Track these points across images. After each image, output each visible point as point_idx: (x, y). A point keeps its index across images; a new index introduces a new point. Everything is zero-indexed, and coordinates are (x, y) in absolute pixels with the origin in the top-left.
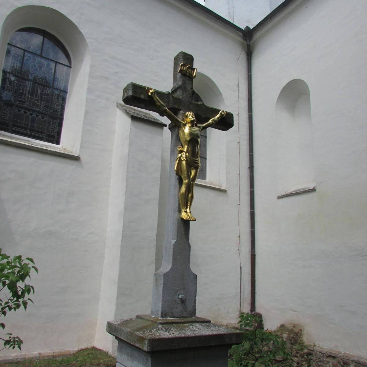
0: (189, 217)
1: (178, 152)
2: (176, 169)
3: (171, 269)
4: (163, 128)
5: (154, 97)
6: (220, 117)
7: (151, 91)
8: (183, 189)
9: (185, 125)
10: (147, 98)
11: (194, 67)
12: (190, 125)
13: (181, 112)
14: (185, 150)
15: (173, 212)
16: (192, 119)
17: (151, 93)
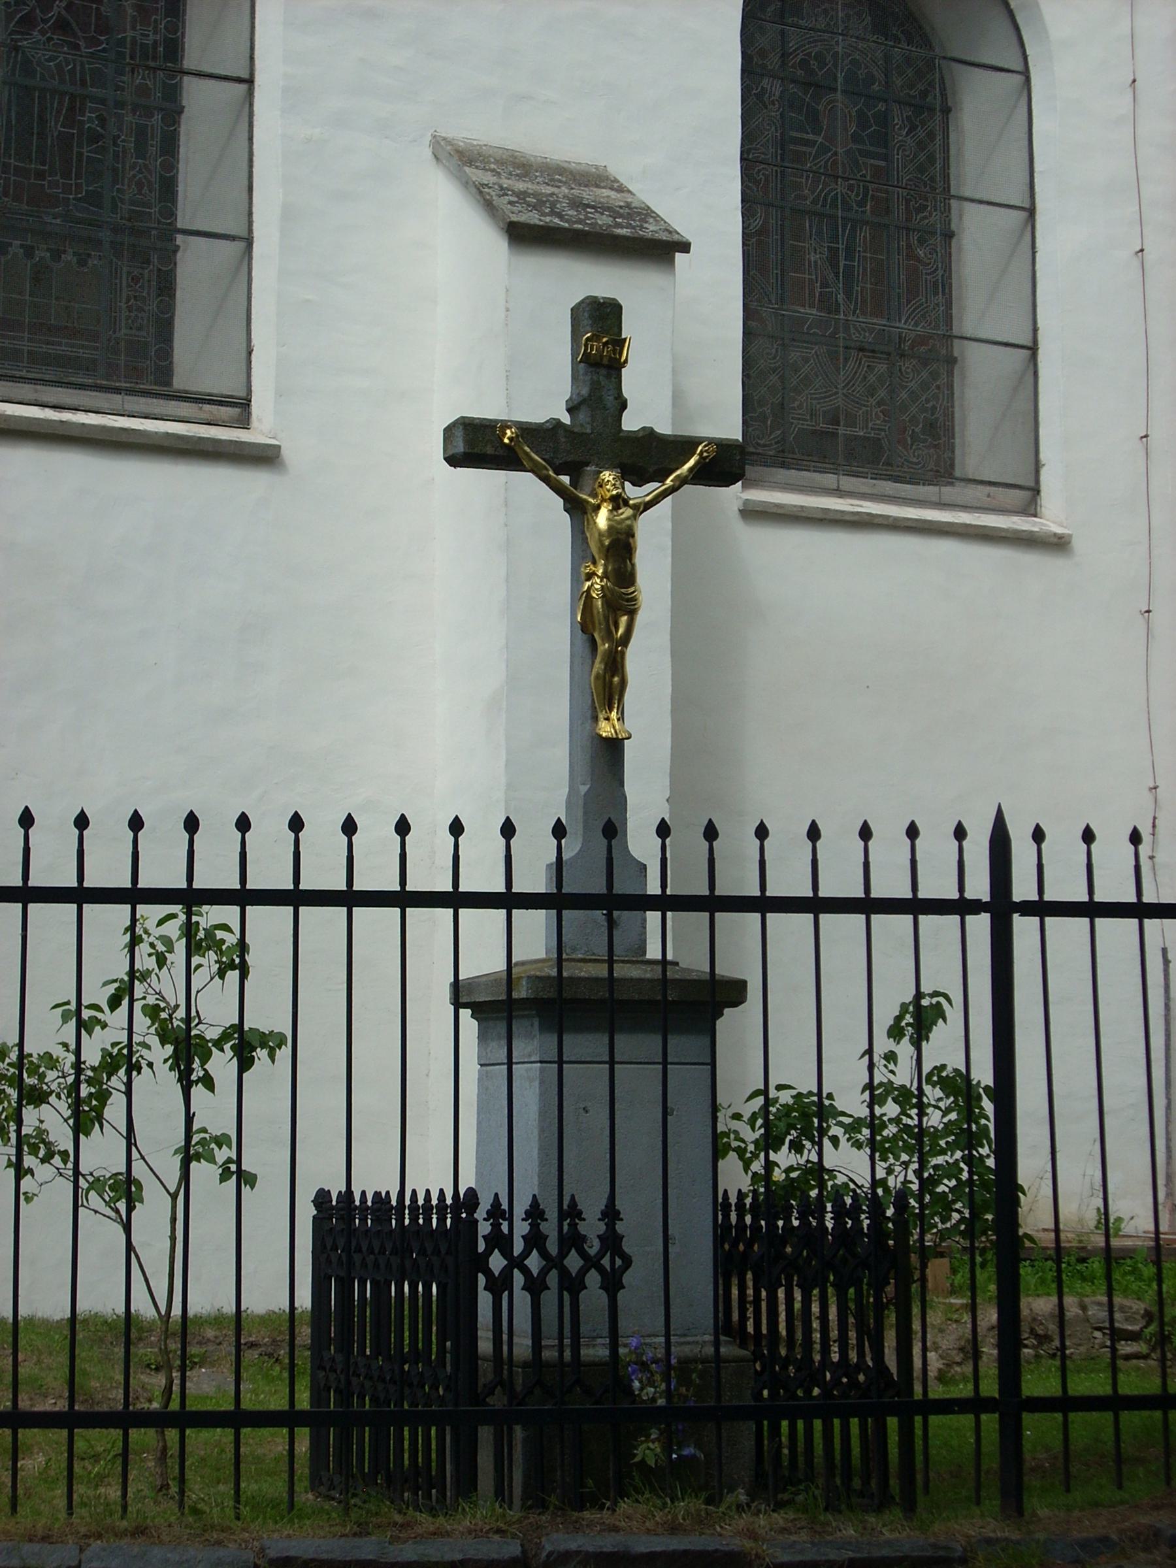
0: (616, 732)
1: (583, 577)
2: (579, 619)
3: (580, 850)
4: (672, 261)
5: (517, 448)
6: (697, 463)
7: (508, 432)
8: (598, 666)
9: (597, 508)
10: (501, 452)
11: (623, 336)
12: (610, 508)
13: (589, 468)
14: (600, 572)
15: (580, 722)
16: (614, 492)
17: (508, 438)
